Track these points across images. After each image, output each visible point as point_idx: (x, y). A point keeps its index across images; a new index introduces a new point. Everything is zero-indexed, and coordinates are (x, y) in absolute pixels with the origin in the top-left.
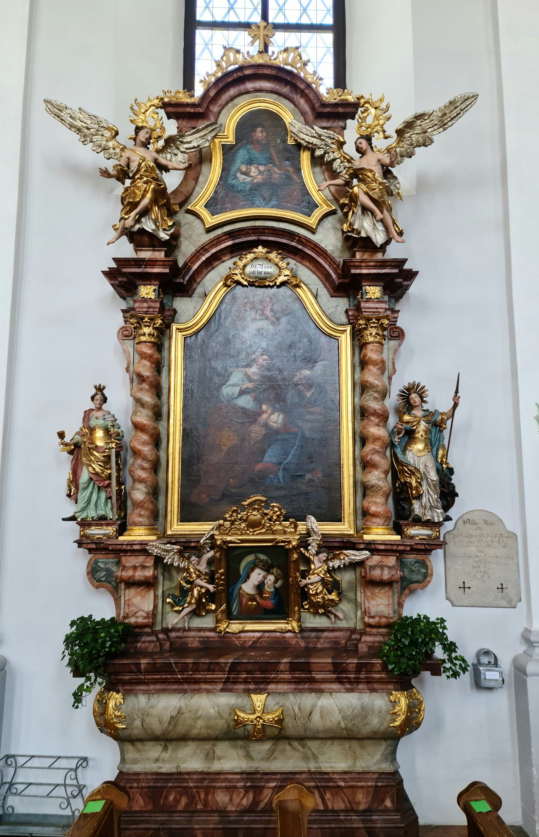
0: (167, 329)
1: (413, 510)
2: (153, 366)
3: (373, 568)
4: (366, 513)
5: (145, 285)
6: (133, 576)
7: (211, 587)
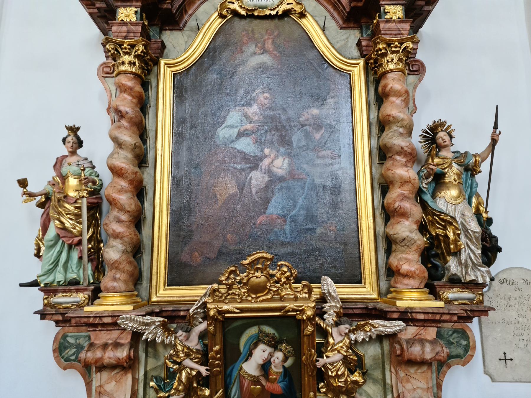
0: (154, 65)
1: (448, 269)
2: (134, 101)
3: (411, 342)
4: (391, 272)
5: (125, 7)
6: (101, 358)
7: (203, 370)
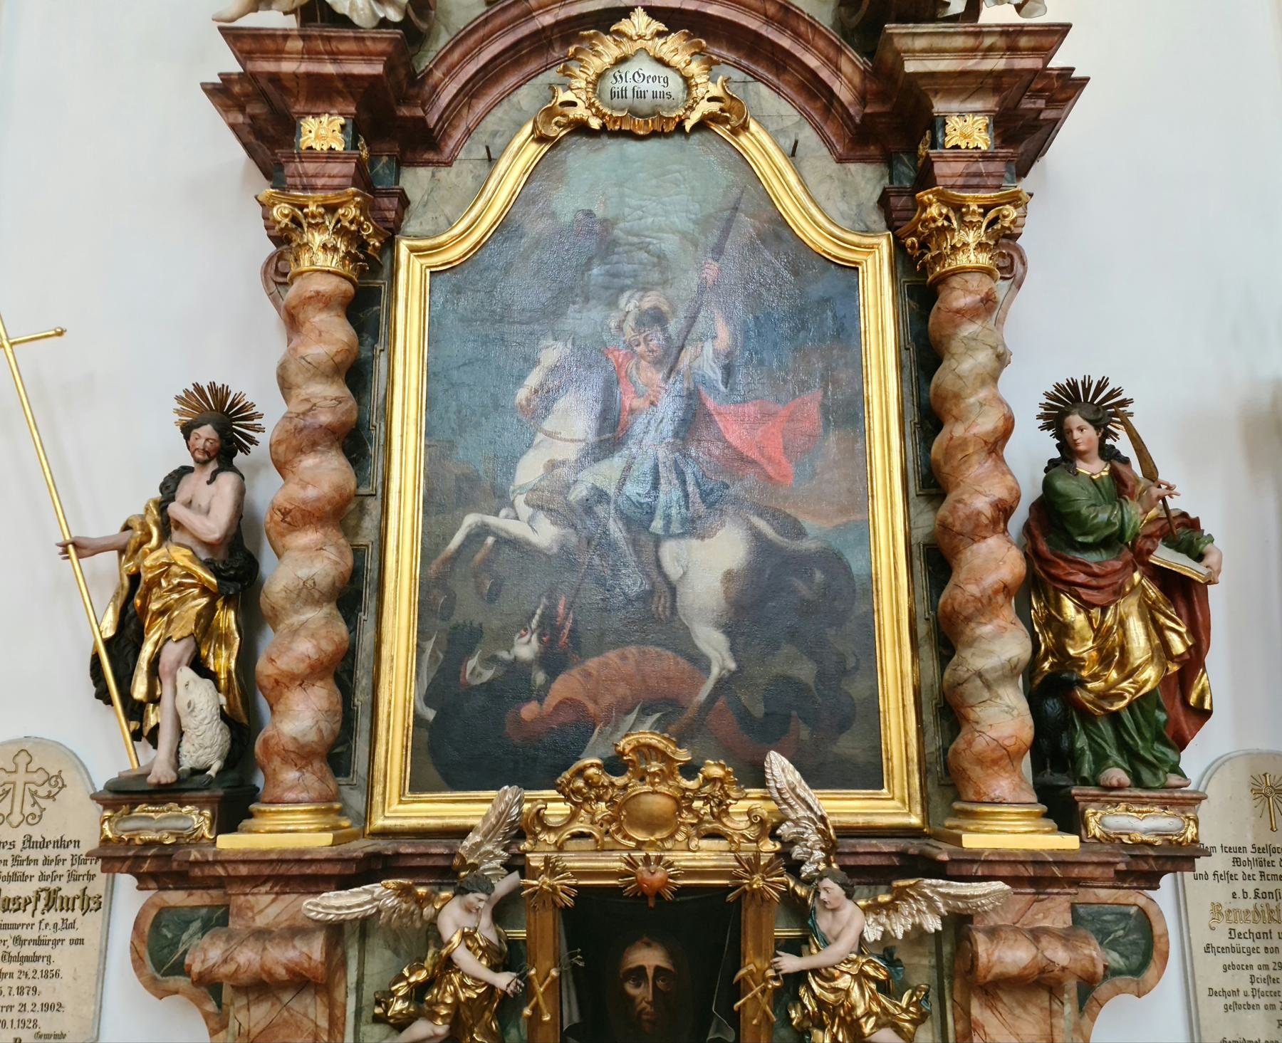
5: (316, 115)
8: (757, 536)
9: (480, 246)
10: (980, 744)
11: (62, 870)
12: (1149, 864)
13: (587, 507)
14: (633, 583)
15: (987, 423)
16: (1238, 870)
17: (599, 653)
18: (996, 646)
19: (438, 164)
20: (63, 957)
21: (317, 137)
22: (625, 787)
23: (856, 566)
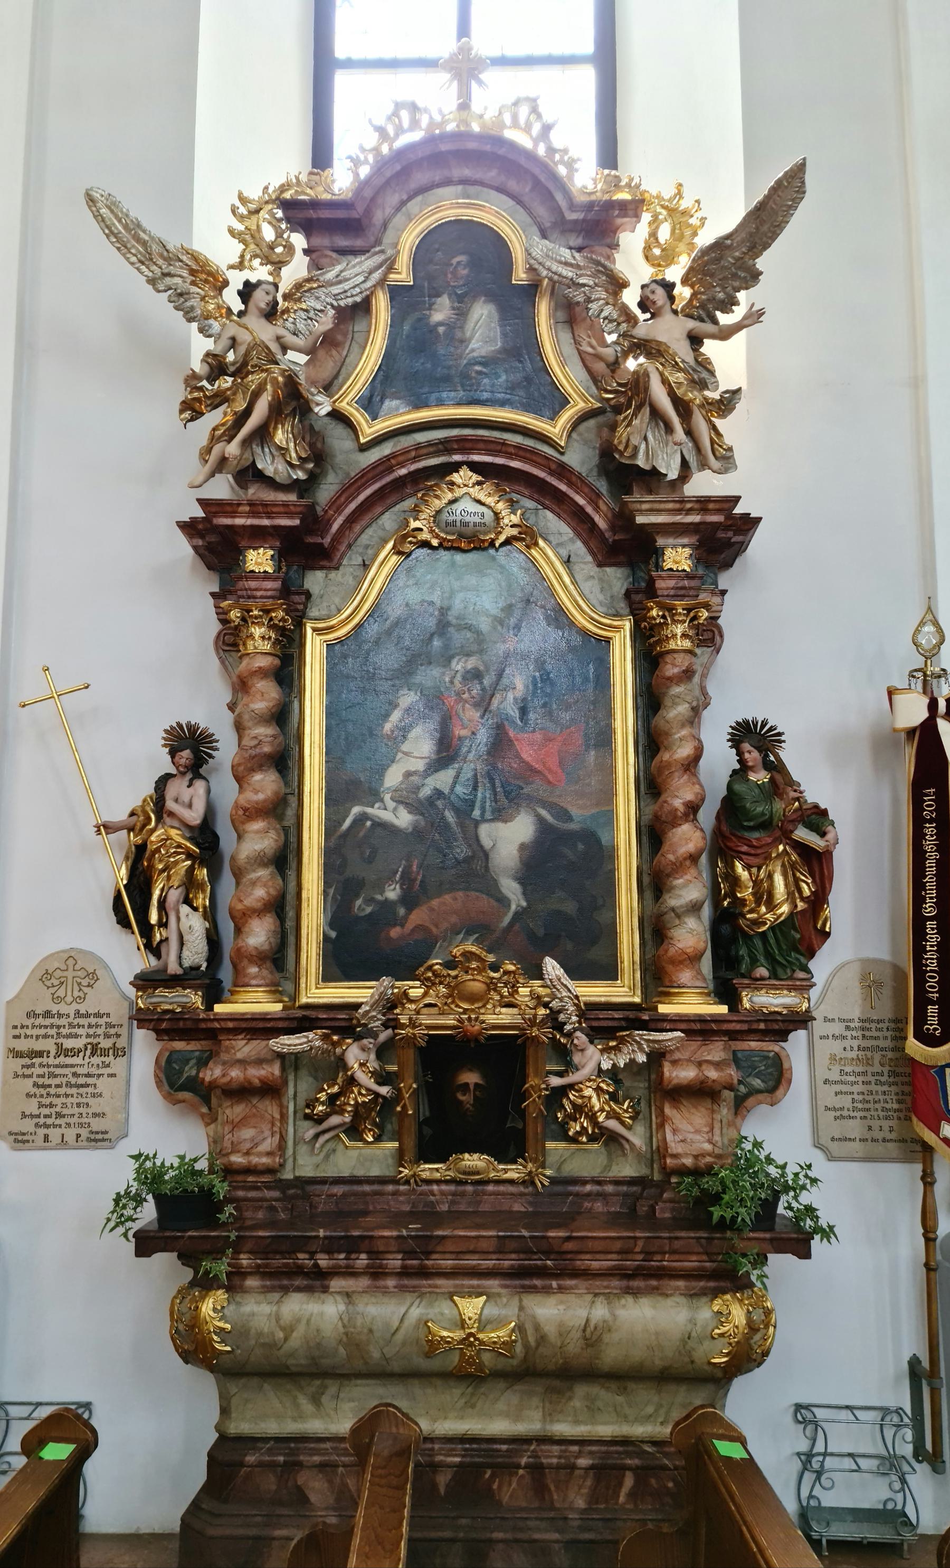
5: (255, 549)
8: (540, 820)
9: (359, 626)
10: (672, 951)
11: (100, 1031)
12: (783, 1025)
13: (430, 801)
14: (461, 851)
15: (684, 751)
16: (848, 1033)
17: (439, 895)
18: (683, 893)
19: (329, 568)
20: (103, 1085)
21: (256, 563)
22: (456, 977)
23: (604, 840)
